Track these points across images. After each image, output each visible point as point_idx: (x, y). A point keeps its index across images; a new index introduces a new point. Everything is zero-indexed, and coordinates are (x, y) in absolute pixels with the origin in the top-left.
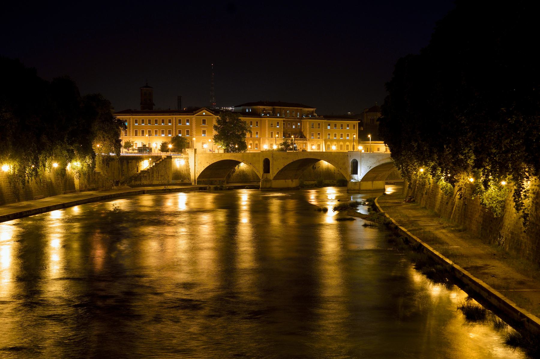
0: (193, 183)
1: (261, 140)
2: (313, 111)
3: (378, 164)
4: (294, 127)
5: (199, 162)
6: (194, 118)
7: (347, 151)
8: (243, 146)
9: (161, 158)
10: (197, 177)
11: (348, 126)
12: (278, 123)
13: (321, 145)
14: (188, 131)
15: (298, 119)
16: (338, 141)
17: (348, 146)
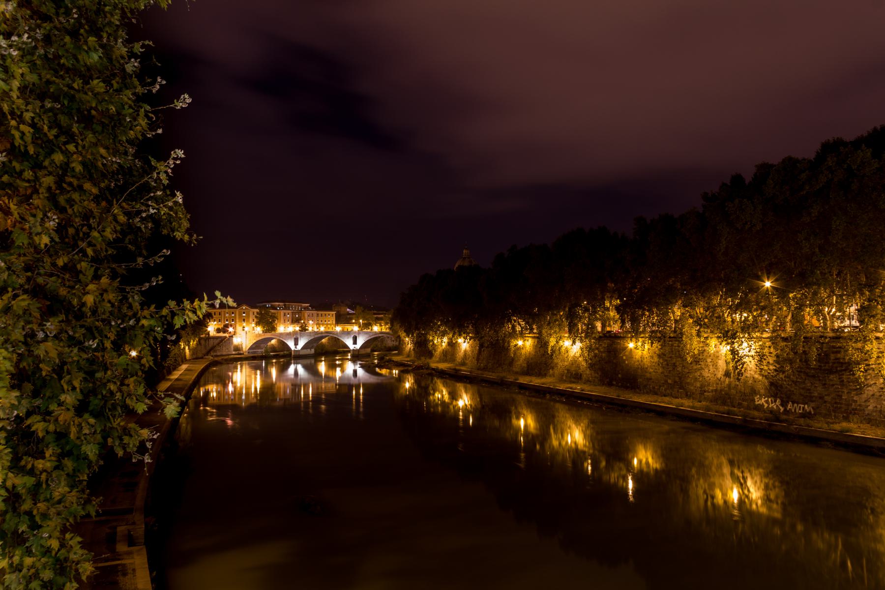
8: (273, 329)
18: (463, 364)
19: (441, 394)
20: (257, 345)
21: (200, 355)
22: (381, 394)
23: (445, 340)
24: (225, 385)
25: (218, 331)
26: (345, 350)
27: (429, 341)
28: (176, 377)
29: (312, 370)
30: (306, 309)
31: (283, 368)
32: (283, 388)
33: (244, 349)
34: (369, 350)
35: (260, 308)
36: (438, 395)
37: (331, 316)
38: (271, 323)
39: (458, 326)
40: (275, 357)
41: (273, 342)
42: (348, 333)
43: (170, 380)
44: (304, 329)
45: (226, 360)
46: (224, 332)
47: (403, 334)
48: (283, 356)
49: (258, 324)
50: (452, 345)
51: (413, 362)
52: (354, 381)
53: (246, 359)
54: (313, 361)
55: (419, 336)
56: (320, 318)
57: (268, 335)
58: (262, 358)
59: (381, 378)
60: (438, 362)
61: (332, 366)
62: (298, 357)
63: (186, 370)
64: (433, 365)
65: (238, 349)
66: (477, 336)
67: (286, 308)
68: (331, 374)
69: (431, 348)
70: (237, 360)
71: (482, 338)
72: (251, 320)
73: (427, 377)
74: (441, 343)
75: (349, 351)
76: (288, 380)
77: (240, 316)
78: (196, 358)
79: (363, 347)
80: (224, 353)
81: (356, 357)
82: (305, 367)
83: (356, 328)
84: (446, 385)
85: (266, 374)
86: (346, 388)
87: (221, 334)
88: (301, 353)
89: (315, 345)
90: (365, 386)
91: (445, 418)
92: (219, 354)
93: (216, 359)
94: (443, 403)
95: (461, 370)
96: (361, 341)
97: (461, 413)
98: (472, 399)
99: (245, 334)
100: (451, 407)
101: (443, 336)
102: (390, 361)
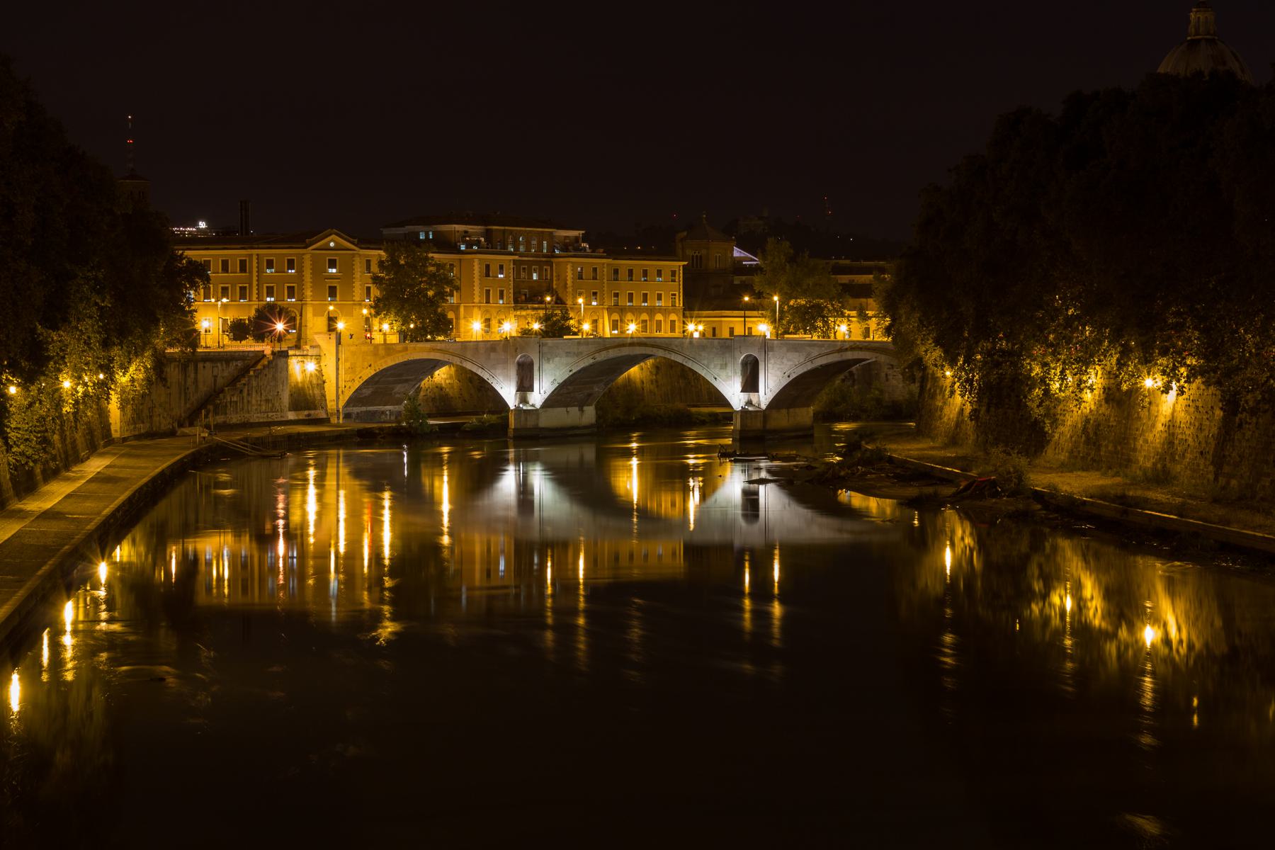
0: (334, 420)
1: (462, 309)
2: (577, 239)
3: (809, 367)
4: (535, 277)
5: (348, 365)
6: (307, 256)
7: (670, 335)
8: (443, 325)
9: (264, 356)
10: (341, 404)
11: (659, 273)
12: (501, 267)
13: (600, 321)
14: (291, 290)
15: (545, 256)
16: (636, 311)
17: (673, 322)
18: (1161, 477)
19: (1076, 596)
20: (379, 387)
21: (164, 424)
22: (845, 582)
23: (1095, 378)
24: (265, 540)
25: (238, 330)
26: (712, 411)
27: (1030, 383)
28: (47, 505)
29: (588, 487)
30: (570, 248)
31: (478, 480)
32: (483, 557)
33: (331, 405)
34: (805, 415)
35: (391, 244)
36: (1064, 601)
37: (664, 281)
38: (432, 303)
39: (1142, 329)
40: (445, 434)
41: (442, 375)
42: (721, 346)
43: (20, 515)
44: (556, 328)
45: (259, 444)
46: (260, 338)
47: (932, 354)
48: (478, 434)
49: (380, 307)
50: (1122, 400)
51: (965, 463)
52: (746, 533)
53: (339, 440)
54: (589, 453)
55: (994, 361)
56: (625, 286)
57: (419, 351)
58: (397, 436)
59: (850, 525)
60: (1063, 468)
61: (670, 475)
62: (531, 437)
63: (99, 479)
64: (1039, 480)
65: (305, 400)
66: (1217, 368)
67: (493, 244)
68: (665, 503)
69: (1037, 412)
70: (299, 444)
71: (1229, 373)
72: (358, 292)
73: (1026, 529)
74: (1080, 390)
75: (729, 417)
76: (491, 524)
77: (318, 273)
78: (147, 429)
79: (782, 400)
80: (255, 418)
81: (754, 438)
82: (560, 476)
83: (764, 328)
84: (1092, 559)
85: (414, 499)
86: (713, 559)
87: (249, 345)
88: (546, 421)
89: (598, 390)
90: (795, 554)
91: (1096, 681)
92: (235, 419)
93: (219, 438)
94: (1082, 630)
95: (1146, 503)
96: (770, 385)
97: (1148, 682)
98: (1193, 620)
99: (335, 348)
100: (1111, 648)
101: (1085, 362)
102: (878, 459)
